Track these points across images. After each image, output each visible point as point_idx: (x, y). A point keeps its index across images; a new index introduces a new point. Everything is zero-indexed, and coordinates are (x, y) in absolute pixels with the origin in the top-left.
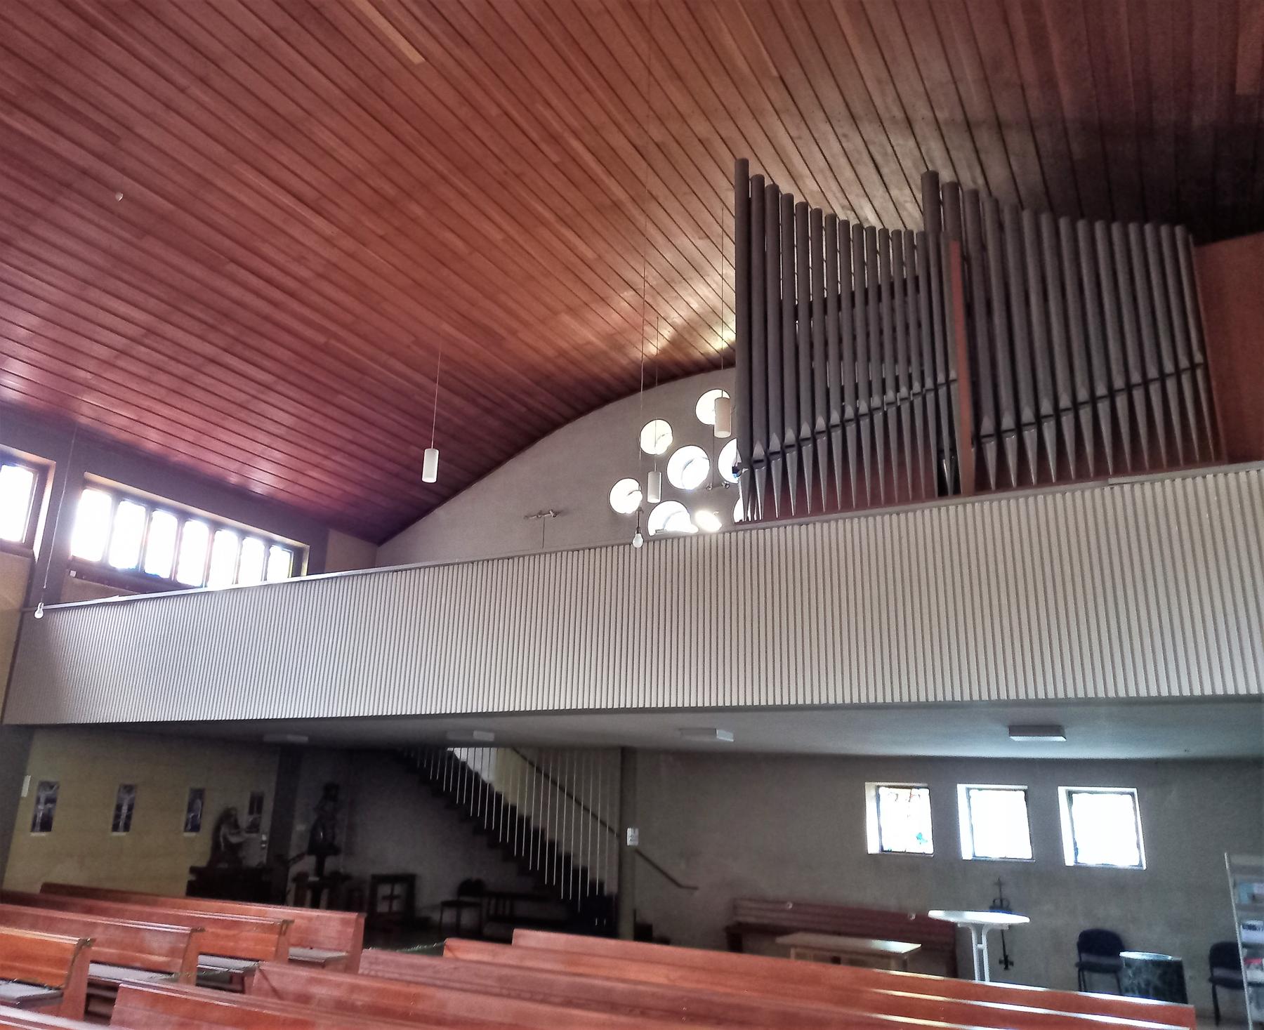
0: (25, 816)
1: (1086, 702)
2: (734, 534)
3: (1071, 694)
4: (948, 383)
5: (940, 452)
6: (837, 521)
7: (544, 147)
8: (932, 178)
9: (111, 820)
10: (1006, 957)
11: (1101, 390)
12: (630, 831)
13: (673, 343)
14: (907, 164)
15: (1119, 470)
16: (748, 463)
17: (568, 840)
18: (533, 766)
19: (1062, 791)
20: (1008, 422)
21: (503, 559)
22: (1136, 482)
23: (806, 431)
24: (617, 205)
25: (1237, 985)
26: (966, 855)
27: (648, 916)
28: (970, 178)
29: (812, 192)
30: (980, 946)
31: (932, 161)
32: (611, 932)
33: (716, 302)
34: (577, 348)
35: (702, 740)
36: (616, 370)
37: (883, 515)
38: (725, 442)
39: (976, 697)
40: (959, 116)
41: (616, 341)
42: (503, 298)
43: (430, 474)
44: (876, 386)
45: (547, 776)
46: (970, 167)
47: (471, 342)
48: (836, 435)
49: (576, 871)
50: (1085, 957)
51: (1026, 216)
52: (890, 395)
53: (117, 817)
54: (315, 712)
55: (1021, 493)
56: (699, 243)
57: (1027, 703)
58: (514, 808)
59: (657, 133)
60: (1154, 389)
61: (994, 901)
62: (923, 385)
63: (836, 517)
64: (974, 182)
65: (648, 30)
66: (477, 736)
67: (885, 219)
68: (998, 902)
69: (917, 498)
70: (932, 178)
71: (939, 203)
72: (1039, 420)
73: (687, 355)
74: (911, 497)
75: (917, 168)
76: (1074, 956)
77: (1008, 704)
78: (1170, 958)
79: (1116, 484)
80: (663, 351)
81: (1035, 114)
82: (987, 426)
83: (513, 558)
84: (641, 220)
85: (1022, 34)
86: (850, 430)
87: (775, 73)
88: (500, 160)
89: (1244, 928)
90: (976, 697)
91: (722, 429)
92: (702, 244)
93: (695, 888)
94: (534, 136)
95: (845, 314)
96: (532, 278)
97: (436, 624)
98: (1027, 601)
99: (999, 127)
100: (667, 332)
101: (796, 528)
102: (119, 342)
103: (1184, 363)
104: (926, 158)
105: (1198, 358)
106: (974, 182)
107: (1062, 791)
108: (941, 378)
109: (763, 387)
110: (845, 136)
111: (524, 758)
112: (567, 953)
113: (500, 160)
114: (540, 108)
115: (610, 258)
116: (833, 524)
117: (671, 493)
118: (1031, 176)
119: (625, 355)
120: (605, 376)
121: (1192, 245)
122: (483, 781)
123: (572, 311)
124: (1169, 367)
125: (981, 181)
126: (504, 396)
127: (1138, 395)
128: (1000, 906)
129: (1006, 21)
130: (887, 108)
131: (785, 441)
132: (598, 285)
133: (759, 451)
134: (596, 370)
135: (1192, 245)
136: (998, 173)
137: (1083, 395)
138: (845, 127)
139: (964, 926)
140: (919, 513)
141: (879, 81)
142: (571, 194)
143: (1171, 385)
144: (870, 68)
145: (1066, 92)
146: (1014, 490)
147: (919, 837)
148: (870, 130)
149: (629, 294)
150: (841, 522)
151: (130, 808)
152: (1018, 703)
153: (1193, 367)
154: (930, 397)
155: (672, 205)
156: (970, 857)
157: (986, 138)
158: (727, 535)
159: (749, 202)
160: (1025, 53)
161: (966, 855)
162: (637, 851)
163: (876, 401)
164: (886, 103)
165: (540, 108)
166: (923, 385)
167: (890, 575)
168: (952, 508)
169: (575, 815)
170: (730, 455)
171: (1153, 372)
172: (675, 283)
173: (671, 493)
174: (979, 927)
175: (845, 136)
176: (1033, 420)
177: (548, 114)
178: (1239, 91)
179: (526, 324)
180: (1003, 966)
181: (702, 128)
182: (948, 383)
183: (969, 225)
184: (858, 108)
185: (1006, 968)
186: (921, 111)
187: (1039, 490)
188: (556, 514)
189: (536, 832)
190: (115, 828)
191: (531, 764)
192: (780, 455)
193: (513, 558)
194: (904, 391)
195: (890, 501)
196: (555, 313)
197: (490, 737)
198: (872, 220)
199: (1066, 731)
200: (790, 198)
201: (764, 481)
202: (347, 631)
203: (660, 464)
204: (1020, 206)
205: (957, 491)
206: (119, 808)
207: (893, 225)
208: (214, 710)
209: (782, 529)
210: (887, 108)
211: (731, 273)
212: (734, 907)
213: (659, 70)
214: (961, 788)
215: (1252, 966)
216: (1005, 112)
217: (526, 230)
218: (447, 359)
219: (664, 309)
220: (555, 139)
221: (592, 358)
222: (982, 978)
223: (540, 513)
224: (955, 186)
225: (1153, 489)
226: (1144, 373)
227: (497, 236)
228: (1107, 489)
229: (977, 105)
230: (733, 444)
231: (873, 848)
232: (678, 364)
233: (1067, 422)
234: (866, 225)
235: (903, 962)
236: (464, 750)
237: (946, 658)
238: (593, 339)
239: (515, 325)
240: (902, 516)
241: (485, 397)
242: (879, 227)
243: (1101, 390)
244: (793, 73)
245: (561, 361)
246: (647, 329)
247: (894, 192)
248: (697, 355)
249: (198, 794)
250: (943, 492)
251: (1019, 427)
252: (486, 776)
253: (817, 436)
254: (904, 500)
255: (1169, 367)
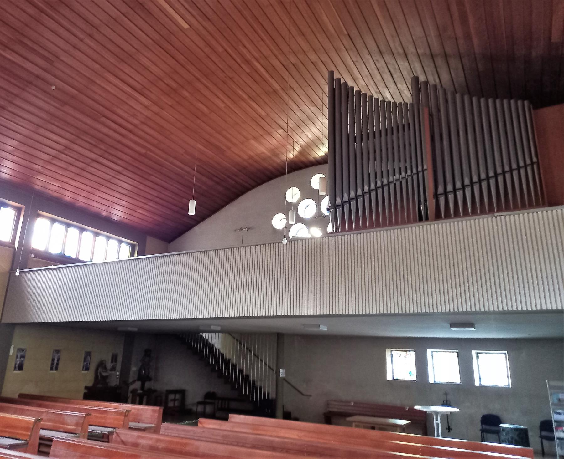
0: (11, 364)
1: (485, 313)
2: (327, 238)
3: (478, 309)
4: (423, 171)
5: (419, 201)
6: (373, 232)
7: (243, 65)
8: (416, 80)
9: (49, 366)
10: (449, 426)
11: (491, 174)
12: (281, 370)
13: (300, 153)
14: (405, 73)
15: (499, 210)
16: (334, 206)
17: (253, 374)
18: (238, 341)
19: (474, 353)
20: (450, 188)
21: (224, 249)
22: (507, 215)
23: (359, 192)
24: (275, 91)
25: (552, 439)
26: (431, 381)
27: (289, 408)
28: (433, 79)
29: (362, 86)
30: (437, 422)
31: (416, 72)
32: (272, 415)
33: (319, 135)
34: (257, 155)
35: (313, 330)
36: (275, 165)
37: (394, 230)
38: (323, 197)
39: (435, 311)
40: (428, 52)
41: (275, 152)
42: (224, 133)
43: (192, 211)
44: (391, 172)
45: (244, 346)
46: (433, 74)
47: (210, 152)
48: (373, 194)
49: (257, 388)
50: (484, 427)
51: (458, 96)
52: (397, 176)
53: (52, 364)
54: (140, 317)
55: (455, 220)
56: (312, 108)
57: (458, 313)
58: (229, 360)
59: (293, 59)
60: (515, 173)
61: (444, 402)
62: (412, 172)
63: (373, 231)
64: (435, 81)
65: (289, 14)
66: (213, 328)
67: (395, 97)
68: (445, 402)
69: (409, 222)
70: (416, 80)
71: (419, 90)
72: (463, 187)
73: (307, 158)
74: (406, 221)
75: (409, 75)
76: (479, 426)
77: (450, 314)
78: (522, 427)
79: (498, 216)
80: (296, 156)
81: (462, 51)
82: (441, 190)
83: (229, 249)
84: (286, 98)
85: (456, 15)
86: (379, 191)
87: (346, 33)
88: (223, 71)
89: (555, 413)
90: (435, 311)
91: (322, 191)
92: (313, 109)
93: (310, 396)
94: (238, 60)
95: (377, 140)
96: (237, 124)
97: (195, 278)
98: (458, 268)
99: (446, 57)
100: (298, 148)
101: (355, 235)
102: (53, 152)
103: (528, 162)
104: (413, 70)
105: (535, 159)
106: (435, 81)
107: (474, 353)
108: (420, 169)
109: (341, 173)
110: (377, 60)
111: (234, 338)
112: (253, 424)
113: (223, 71)
114: (241, 48)
115: (272, 115)
116: (372, 234)
117: (299, 220)
118: (460, 78)
119: (279, 158)
120: (270, 167)
121: (532, 109)
122: (216, 348)
123: (255, 138)
124: (522, 164)
125: (438, 81)
126: (225, 176)
127: (508, 176)
128: (446, 404)
129: (449, 9)
130: (396, 48)
131: (350, 196)
132: (267, 127)
133: (338, 201)
134: (266, 165)
135: (532, 109)
136: (445, 77)
137: (483, 176)
138: (377, 57)
139: (430, 413)
140: (410, 229)
141: (392, 36)
142: (255, 86)
143: (522, 171)
144: (388, 30)
145: (476, 41)
146: (453, 218)
147: (410, 373)
148: (388, 58)
149: (281, 131)
150: (375, 233)
151: (58, 360)
152: (454, 313)
153: (532, 164)
154: (415, 177)
155: (300, 91)
156: (433, 382)
157: (440, 62)
158: (324, 238)
159: (334, 90)
160: (457, 23)
161: (431, 381)
162: (284, 379)
163: (391, 179)
164: (395, 46)
165: (241, 48)
166: (412, 172)
167: (397, 256)
168: (425, 227)
169: (257, 363)
170: (326, 203)
171: (514, 166)
172: (301, 126)
173: (299, 220)
174: (437, 413)
175: (377, 60)
176: (461, 187)
177: (244, 51)
178: (553, 41)
179: (235, 145)
180: (448, 431)
181: (313, 57)
182: (423, 171)
183: (432, 100)
184: (383, 48)
185: (449, 431)
186: (411, 49)
187: (464, 218)
188: (248, 229)
189: (239, 371)
190: (52, 369)
191: (237, 340)
192: (348, 203)
193: (229, 249)
194: (403, 174)
195: (397, 223)
196: (248, 140)
197: (219, 328)
198: (389, 98)
199: (476, 326)
200: (352, 88)
201: (341, 214)
202: (155, 281)
203: (294, 207)
204: (455, 92)
205: (427, 219)
206: (53, 360)
207: (398, 100)
208: (95, 317)
209: (349, 236)
210: (396, 48)
211: (326, 122)
212: (328, 404)
213: (294, 31)
214: (429, 351)
215: (559, 431)
216: (449, 50)
217: (235, 103)
218: (199, 160)
219: (296, 138)
220: (248, 62)
221: (264, 159)
222: (438, 436)
223: (241, 229)
224: (426, 83)
225: (514, 218)
226: (510, 166)
227: (222, 105)
228: (494, 218)
229: (436, 47)
230: (327, 198)
231: (389, 378)
232: (302, 162)
233: (476, 188)
234: (386, 100)
235: (403, 429)
236: (207, 334)
237: (422, 293)
238: (265, 151)
239: (230, 145)
240: (403, 230)
241: (216, 177)
242: (392, 101)
243: (491, 174)
244: (354, 33)
245: (250, 161)
246: (289, 146)
247: (399, 86)
248: (311, 158)
249: (88, 354)
250: (421, 219)
251: (455, 190)
252: (217, 346)
253: (365, 194)
254: (403, 223)
255: (522, 164)
